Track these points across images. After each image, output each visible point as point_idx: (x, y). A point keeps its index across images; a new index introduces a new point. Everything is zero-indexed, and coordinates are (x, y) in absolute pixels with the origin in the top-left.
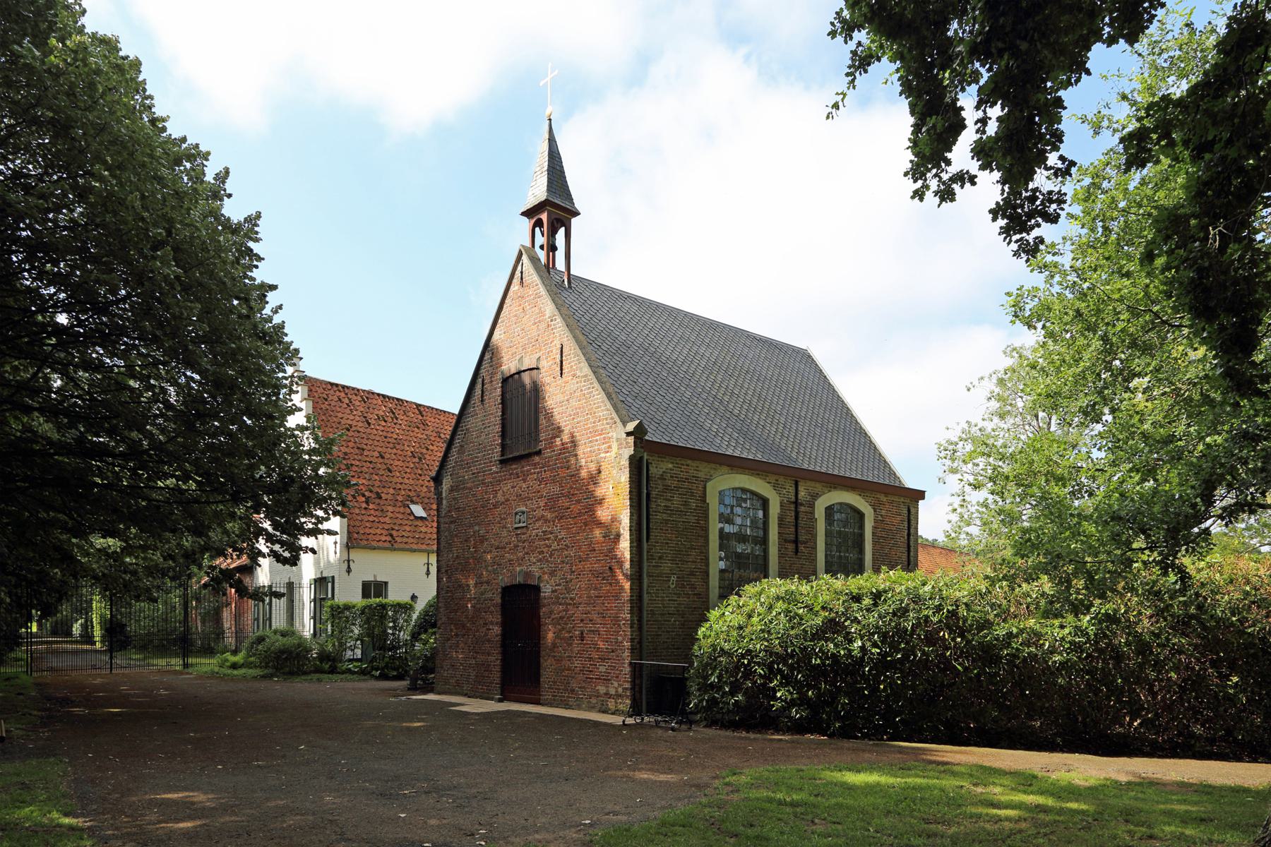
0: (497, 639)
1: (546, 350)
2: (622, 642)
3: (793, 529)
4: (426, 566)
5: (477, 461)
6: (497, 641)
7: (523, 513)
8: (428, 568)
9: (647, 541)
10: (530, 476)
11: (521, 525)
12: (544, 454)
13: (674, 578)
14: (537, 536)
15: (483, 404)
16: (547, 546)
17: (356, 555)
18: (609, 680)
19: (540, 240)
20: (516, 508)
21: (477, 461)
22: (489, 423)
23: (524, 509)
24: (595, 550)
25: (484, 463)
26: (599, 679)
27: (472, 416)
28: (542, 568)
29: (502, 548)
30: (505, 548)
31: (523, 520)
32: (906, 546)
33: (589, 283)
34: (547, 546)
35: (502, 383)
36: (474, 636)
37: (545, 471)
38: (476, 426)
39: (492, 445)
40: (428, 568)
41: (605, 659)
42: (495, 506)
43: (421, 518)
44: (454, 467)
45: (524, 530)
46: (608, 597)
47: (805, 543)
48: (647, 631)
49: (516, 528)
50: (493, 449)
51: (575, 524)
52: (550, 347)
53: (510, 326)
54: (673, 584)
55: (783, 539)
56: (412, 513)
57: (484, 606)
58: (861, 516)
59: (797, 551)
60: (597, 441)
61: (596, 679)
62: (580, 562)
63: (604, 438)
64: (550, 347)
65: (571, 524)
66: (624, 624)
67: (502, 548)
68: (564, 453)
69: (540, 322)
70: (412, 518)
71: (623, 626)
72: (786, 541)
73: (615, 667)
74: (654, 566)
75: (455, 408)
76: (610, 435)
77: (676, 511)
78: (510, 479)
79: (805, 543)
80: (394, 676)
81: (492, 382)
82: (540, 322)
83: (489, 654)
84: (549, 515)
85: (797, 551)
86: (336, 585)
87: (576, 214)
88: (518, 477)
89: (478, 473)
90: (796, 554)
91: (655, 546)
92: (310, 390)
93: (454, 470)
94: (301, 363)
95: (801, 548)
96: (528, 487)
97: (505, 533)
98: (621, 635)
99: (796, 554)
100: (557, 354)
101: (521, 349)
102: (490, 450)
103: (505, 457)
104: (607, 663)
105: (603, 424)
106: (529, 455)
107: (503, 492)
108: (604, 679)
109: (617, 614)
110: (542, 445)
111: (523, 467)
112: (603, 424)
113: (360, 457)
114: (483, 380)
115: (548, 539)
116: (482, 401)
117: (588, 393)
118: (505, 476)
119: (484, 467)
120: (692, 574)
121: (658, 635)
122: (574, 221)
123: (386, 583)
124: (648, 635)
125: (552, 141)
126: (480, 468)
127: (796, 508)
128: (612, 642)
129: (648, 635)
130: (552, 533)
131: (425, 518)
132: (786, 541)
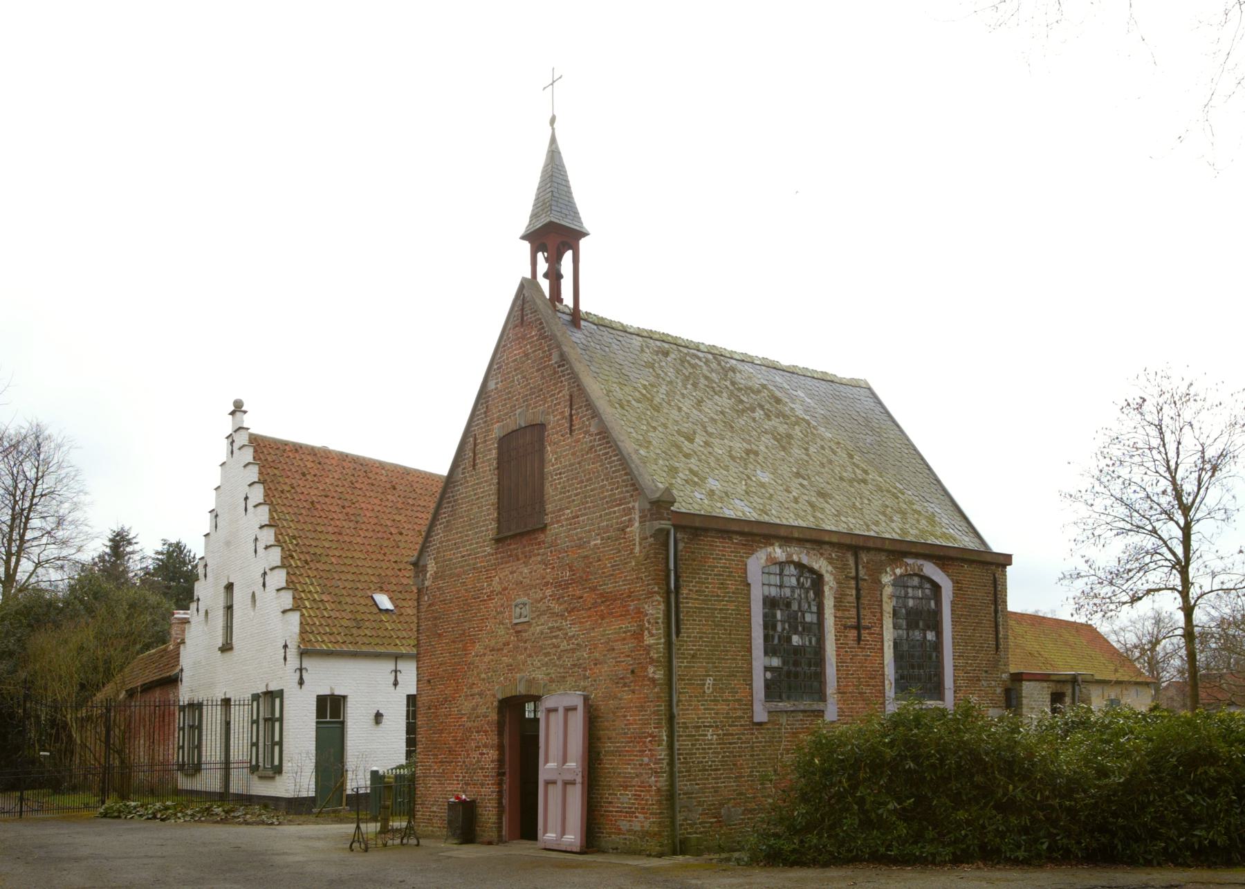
0: (492, 765)
1: (552, 401)
2: (648, 764)
3: (853, 612)
4: (393, 673)
5: (468, 541)
6: (492, 768)
7: (525, 604)
8: (396, 677)
9: (677, 636)
10: (533, 559)
11: (523, 620)
12: (550, 530)
13: (709, 681)
14: (542, 633)
15: (474, 469)
16: (555, 646)
17: (307, 663)
18: (634, 813)
19: (543, 266)
20: (515, 599)
21: (468, 541)
22: (483, 492)
23: (525, 599)
24: (614, 649)
25: (477, 543)
26: (621, 812)
27: (461, 484)
28: (549, 674)
29: (498, 650)
30: (502, 649)
31: (525, 613)
32: (993, 625)
33: (603, 324)
34: (555, 646)
35: (498, 443)
36: (464, 762)
37: (551, 552)
38: (466, 497)
39: (486, 520)
40: (396, 677)
41: (627, 786)
42: (490, 598)
43: (387, 611)
44: (438, 548)
45: (526, 627)
46: (630, 707)
47: (868, 628)
48: (679, 749)
49: (516, 624)
50: (487, 525)
51: (590, 617)
52: (557, 399)
53: (508, 373)
54: (709, 688)
55: (842, 628)
56: (376, 604)
57: (476, 724)
58: (936, 588)
59: (859, 639)
60: (615, 512)
61: (616, 812)
62: (596, 664)
63: (624, 509)
64: (557, 399)
65: (584, 618)
66: (650, 741)
67: (498, 650)
68: (575, 529)
69: (545, 368)
70: (376, 611)
71: (649, 744)
72: (846, 627)
73: (640, 796)
74: (685, 667)
75: (442, 467)
76: (630, 505)
77: (712, 596)
78: (509, 562)
79: (868, 628)
80: (936, 604)
81: (485, 441)
82: (545, 368)
83: (482, 785)
84: (557, 608)
85: (859, 639)
86: (286, 702)
87: (584, 234)
88: (518, 560)
89: (469, 555)
90: (859, 644)
91: (686, 641)
92: (255, 451)
93: (439, 552)
94: (245, 416)
95: (865, 634)
96: (531, 572)
97: (501, 632)
98: (647, 756)
99: (859, 644)
100: (565, 407)
101: (521, 401)
102: (484, 526)
103: (500, 536)
104: (631, 791)
105: (622, 492)
106: (534, 531)
107: (500, 579)
108: (627, 812)
109: (641, 728)
110: (548, 519)
111: (525, 547)
112: (622, 492)
113: (341, 553)
114: (475, 439)
115: (556, 637)
116: (474, 465)
117: (604, 454)
118: (502, 558)
119: (476, 548)
120: (732, 675)
121: (692, 754)
122: (583, 243)
123: (344, 697)
124: (679, 754)
125: (553, 140)
126: (471, 550)
127: (857, 584)
128: (635, 764)
129: (679, 754)
130: (560, 630)
131: (392, 611)
132: (846, 627)
